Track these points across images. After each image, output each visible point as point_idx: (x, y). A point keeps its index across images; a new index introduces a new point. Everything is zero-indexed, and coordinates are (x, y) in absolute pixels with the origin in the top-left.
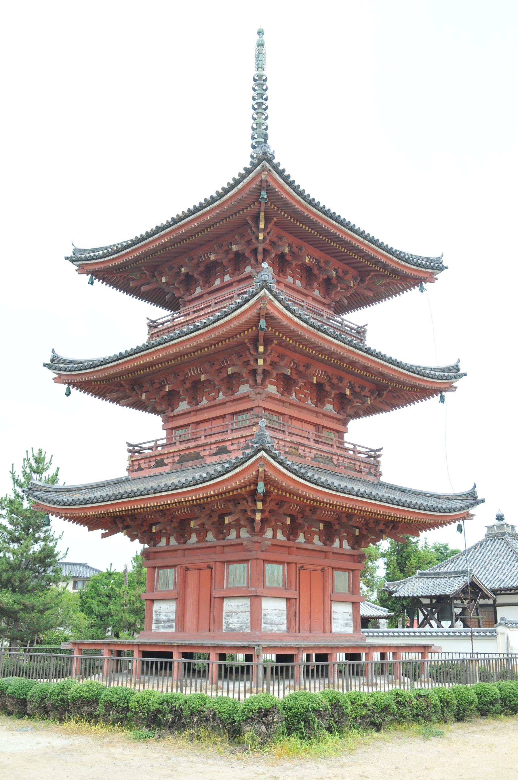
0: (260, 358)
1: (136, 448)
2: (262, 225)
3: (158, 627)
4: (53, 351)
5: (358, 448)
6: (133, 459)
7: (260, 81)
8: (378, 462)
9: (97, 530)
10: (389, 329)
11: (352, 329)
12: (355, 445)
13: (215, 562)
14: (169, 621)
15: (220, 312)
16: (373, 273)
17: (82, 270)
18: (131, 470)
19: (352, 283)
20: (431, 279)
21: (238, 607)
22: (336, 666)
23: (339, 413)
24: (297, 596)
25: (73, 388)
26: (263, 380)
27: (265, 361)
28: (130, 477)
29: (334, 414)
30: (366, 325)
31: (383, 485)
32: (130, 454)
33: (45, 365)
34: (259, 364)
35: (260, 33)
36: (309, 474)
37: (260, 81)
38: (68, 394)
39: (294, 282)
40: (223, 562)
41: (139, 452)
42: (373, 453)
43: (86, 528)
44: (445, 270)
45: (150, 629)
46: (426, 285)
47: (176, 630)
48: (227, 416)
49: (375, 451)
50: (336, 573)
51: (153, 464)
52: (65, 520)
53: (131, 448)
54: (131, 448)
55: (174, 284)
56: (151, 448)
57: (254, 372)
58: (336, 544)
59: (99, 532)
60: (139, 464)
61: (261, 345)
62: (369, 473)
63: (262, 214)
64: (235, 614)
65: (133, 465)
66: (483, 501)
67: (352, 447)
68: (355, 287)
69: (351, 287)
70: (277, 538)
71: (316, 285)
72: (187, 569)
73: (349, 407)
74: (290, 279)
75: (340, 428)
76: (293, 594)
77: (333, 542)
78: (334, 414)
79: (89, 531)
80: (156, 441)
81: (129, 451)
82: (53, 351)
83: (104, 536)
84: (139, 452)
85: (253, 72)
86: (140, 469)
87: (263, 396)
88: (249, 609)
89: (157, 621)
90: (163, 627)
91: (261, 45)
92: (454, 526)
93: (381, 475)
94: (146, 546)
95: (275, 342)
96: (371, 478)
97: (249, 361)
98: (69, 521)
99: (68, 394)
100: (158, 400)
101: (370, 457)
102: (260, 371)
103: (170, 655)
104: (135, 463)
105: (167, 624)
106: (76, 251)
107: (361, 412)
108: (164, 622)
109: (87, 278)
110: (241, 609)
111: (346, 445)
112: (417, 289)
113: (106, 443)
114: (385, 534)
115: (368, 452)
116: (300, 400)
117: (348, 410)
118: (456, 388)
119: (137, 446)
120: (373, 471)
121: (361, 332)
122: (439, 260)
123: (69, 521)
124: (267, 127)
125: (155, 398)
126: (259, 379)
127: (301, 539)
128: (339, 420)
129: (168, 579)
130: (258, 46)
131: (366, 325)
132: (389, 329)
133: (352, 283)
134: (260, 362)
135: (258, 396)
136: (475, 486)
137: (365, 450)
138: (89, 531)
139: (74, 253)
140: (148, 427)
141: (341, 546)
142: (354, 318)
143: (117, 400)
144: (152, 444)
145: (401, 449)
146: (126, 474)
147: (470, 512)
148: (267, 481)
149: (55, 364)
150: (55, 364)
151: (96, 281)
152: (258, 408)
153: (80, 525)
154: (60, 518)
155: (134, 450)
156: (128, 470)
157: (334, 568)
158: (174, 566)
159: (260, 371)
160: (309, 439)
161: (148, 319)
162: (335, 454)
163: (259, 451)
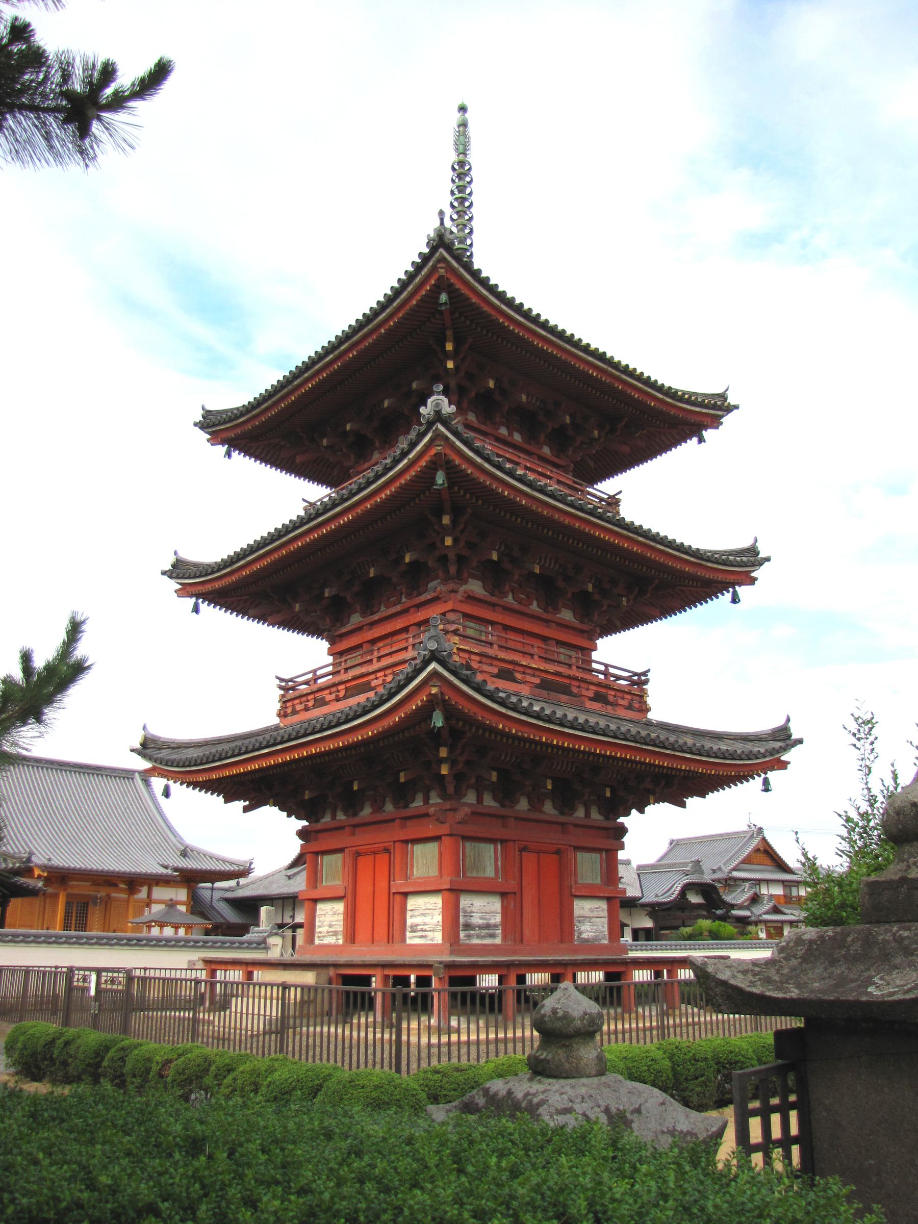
0: (448, 535)
1: (290, 683)
2: (449, 347)
3: (469, 936)
4: (176, 553)
5: (612, 670)
6: (285, 699)
7: (462, 171)
8: (643, 690)
9: (237, 802)
10: (656, 497)
11: (601, 500)
12: (606, 666)
13: (395, 842)
14: (488, 926)
15: (389, 472)
16: (626, 419)
17: (216, 438)
18: (282, 714)
19: (596, 432)
20: (715, 422)
21: (591, 910)
22: (632, 987)
23: (582, 622)
24: (516, 890)
25: (203, 602)
26: (459, 572)
27: (455, 541)
28: (282, 725)
29: (575, 622)
30: (620, 492)
31: (649, 724)
32: (282, 692)
33: (164, 573)
34: (446, 544)
35: (463, 109)
36: (536, 708)
37: (462, 171)
38: (196, 610)
39: (511, 434)
40: (406, 842)
41: (293, 688)
42: (636, 678)
43: (221, 799)
44: (735, 411)
45: (403, 939)
46: (708, 434)
47: (504, 938)
48: (411, 629)
49: (639, 675)
50: (580, 855)
51: (311, 704)
52: (188, 786)
53: (283, 684)
54: (283, 684)
55: (341, 450)
56: (306, 683)
57: (444, 559)
58: (580, 813)
59: (240, 804)
60: (293, 705)
61: (447, 514)
62: (630, 707)
63: (449, 333)
64: (425, 919)
65: (286, 708)
66: (800, 741)
67: (602, 668)
68: (602, 440)
69: (597, 440)
70: (485, 804)
71: (542, 437)
72: (358, 854)
73: (596, 615)
74: (503, 431)
75: (584, 643)
76: (512, 885)
77: (573, 809)
78: (575, 622)
79: (226, 802)
80: (315, 671)
81: (281, 688)
82: (176, 553)
83: (246, 809)
84: (293, 688)
85: (453, 157)
86: (295, 712)
87: (459, 596)
88: (605, 914)
89: (468, 926)
90: (478, 936)
91: (464, 125)
92: (758, 782)
93: (648, 710)
94: (305, 823)
95: (469, 511)
96: (631, 715)
97: (434, 543)
98: (194, 789)
99: (196, 610)
100: (319, 613)
101: (634, 683)
102: (452, 556)
103: (365, 980)
104: (289, 704)
105: (484, 932)
106: (207, 414)
107: (618, 623)
108: (481, 927)
109: (222, 449)
110: (595, 914)
111: (595, 666)
112: (695, 439)
113: (250, 676)
114: (654, 795)
115: (631, 676)
116: (520, 603)
117: (596, 618)
118: (756, 579)
119: (291, 680)
120: (636, 705)
121: (613, 502)
122: (723, 397)
123: (194, 789)
124: (472, 230)
125: (316, 612)
126: (453, 569)
127: (523, 805)
128: (582, 632)
129: (333, 868)
130: (459, 126)
131: (620, 492)
132: (656, 497)
133: (596, 432)
134: (449, 541)
135: (452, 594)
136: (788, 720)
137: (626, 674)
138: (226, 802)
139: (203, 417)
140: (307, 654)
141: (587, 815)
142: (607, 487)
143: (261, 618)
144: (310, 676)
145: (677, 669)
146: (277, 721)
147: (782, 758)
148: (450, 714)
149: (179, 570)
150: (179, 570)
151: (235, 454)
152: (451, 613)
153: (212, 794)
154: (181, 784)
155: (287, 686)
156: (279, 715)
157: (578, 848)
158: (341, 850)
159: (452, 556)
160: (532, 655)
161: (304, 500)
162: (575, 679)
163: (426, 663)
